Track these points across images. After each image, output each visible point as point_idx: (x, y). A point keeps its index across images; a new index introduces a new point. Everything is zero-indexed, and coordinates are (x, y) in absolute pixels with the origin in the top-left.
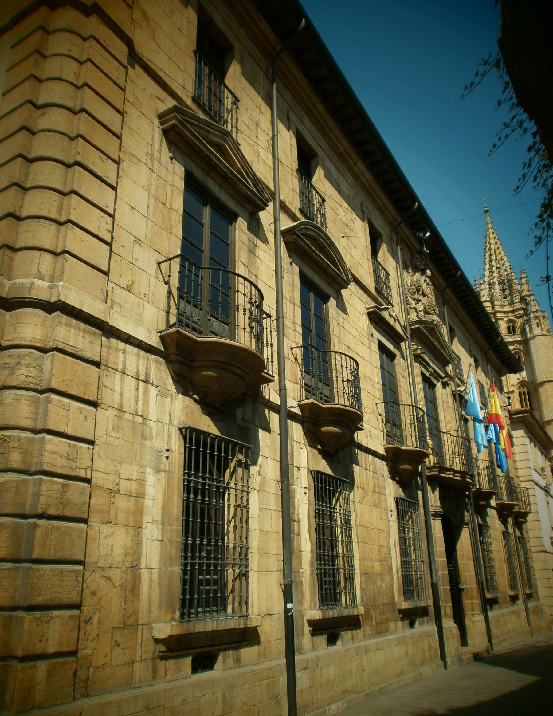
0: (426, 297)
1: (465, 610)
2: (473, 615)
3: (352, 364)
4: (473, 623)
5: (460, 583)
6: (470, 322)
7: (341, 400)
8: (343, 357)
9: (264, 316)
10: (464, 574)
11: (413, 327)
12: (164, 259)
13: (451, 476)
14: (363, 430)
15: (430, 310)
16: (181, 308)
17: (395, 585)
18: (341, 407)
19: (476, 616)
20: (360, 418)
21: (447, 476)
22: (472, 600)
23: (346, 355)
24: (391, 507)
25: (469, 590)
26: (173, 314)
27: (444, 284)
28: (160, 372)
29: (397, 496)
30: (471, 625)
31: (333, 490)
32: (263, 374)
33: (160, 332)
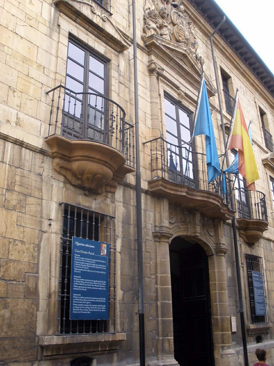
0: (176, 26)
1: (215, 342)
2: (223, 348)
3: (259, 196)
4: (222, 356)
5: (211, 314)
6: (253, 77)
7: (256, 216)
8: (258, 192)
9: (128, 126)
10: (60, 299)
11: (147, 43)
12: (50, 89)
13: (184, 194)
14: (268, 230)
15: (180, 38)
16: (66, 122)
17: (40, 316)
18: (258, 220)
19: (225, 348)
20: (267, 225)
21: (179, 193)
22: (222, 331)
23: (259, 192)
24: (49, 215)
25: (219, 321)
26: (59, 127)
27: (212, 31)
28: (47, 167)
29: (70, 203)
30: (220, 358)
31: (250, 262)
32: (125, 165)
33: (47, 138)
